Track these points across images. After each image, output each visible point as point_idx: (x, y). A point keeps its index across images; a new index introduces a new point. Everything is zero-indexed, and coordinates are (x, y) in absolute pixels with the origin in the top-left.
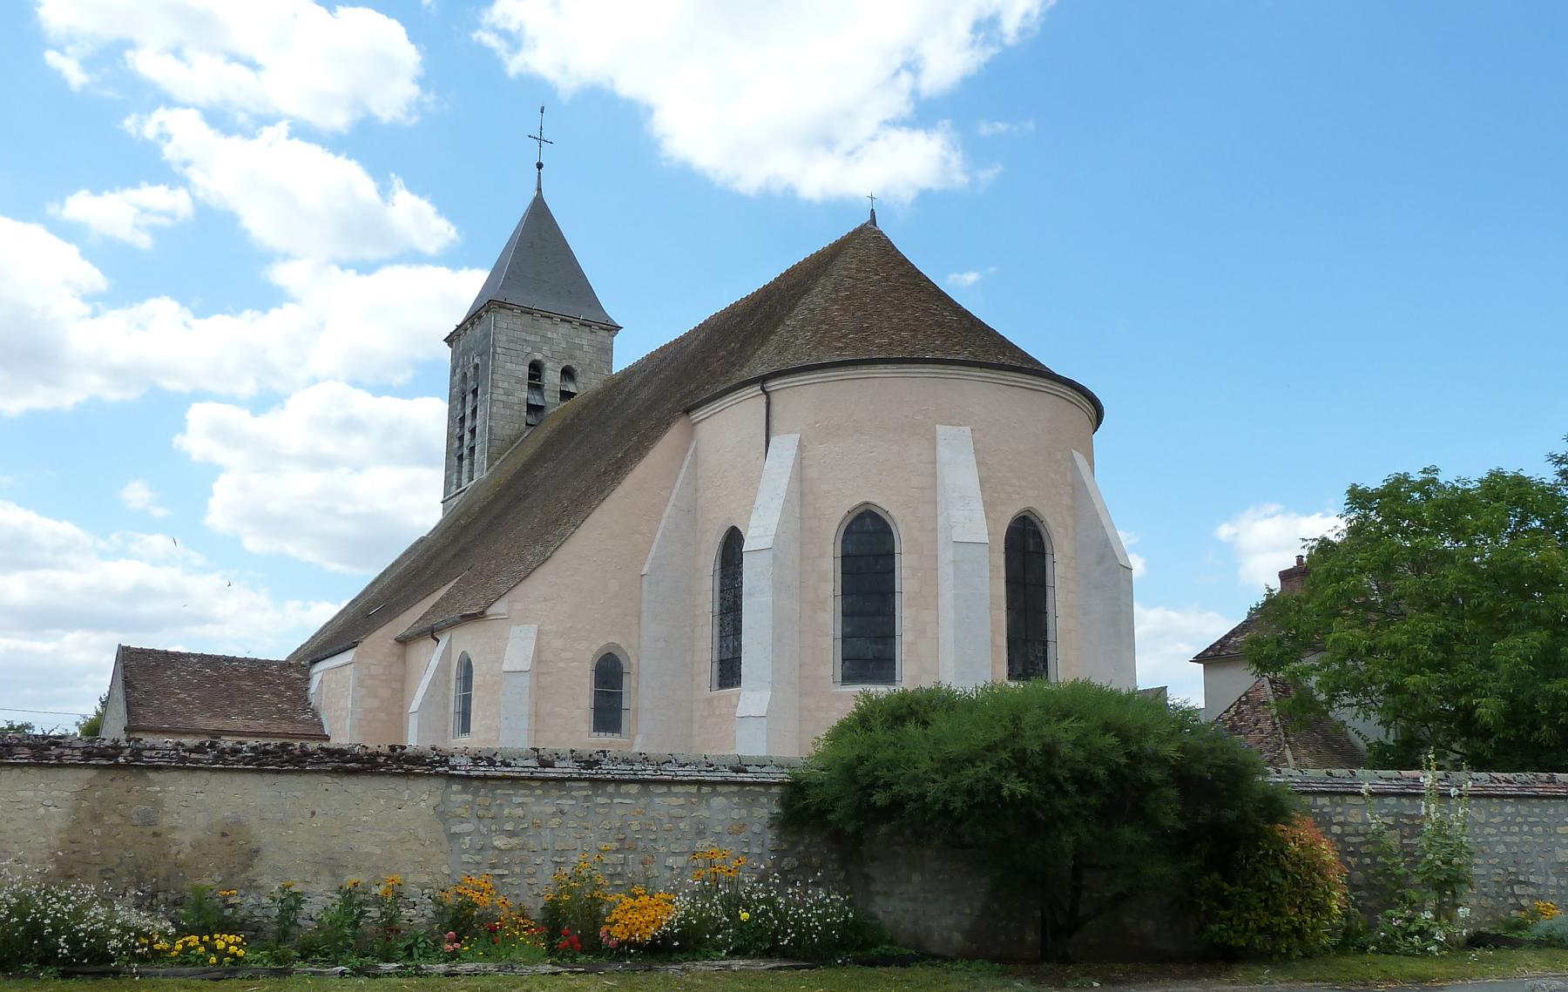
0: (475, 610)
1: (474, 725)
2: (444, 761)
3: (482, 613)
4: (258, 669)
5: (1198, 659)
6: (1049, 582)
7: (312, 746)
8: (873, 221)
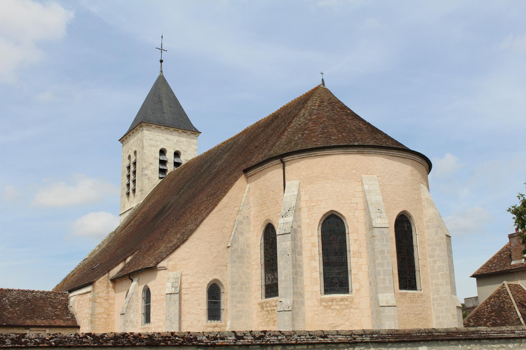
0: (151, 265)
1: (152, 319)
2: (195, 338)
3: (155, 266)
4: (45, 296)
5: (473, 276)
6: (414, 244)
7: (66, 333)
8: (323, 84)
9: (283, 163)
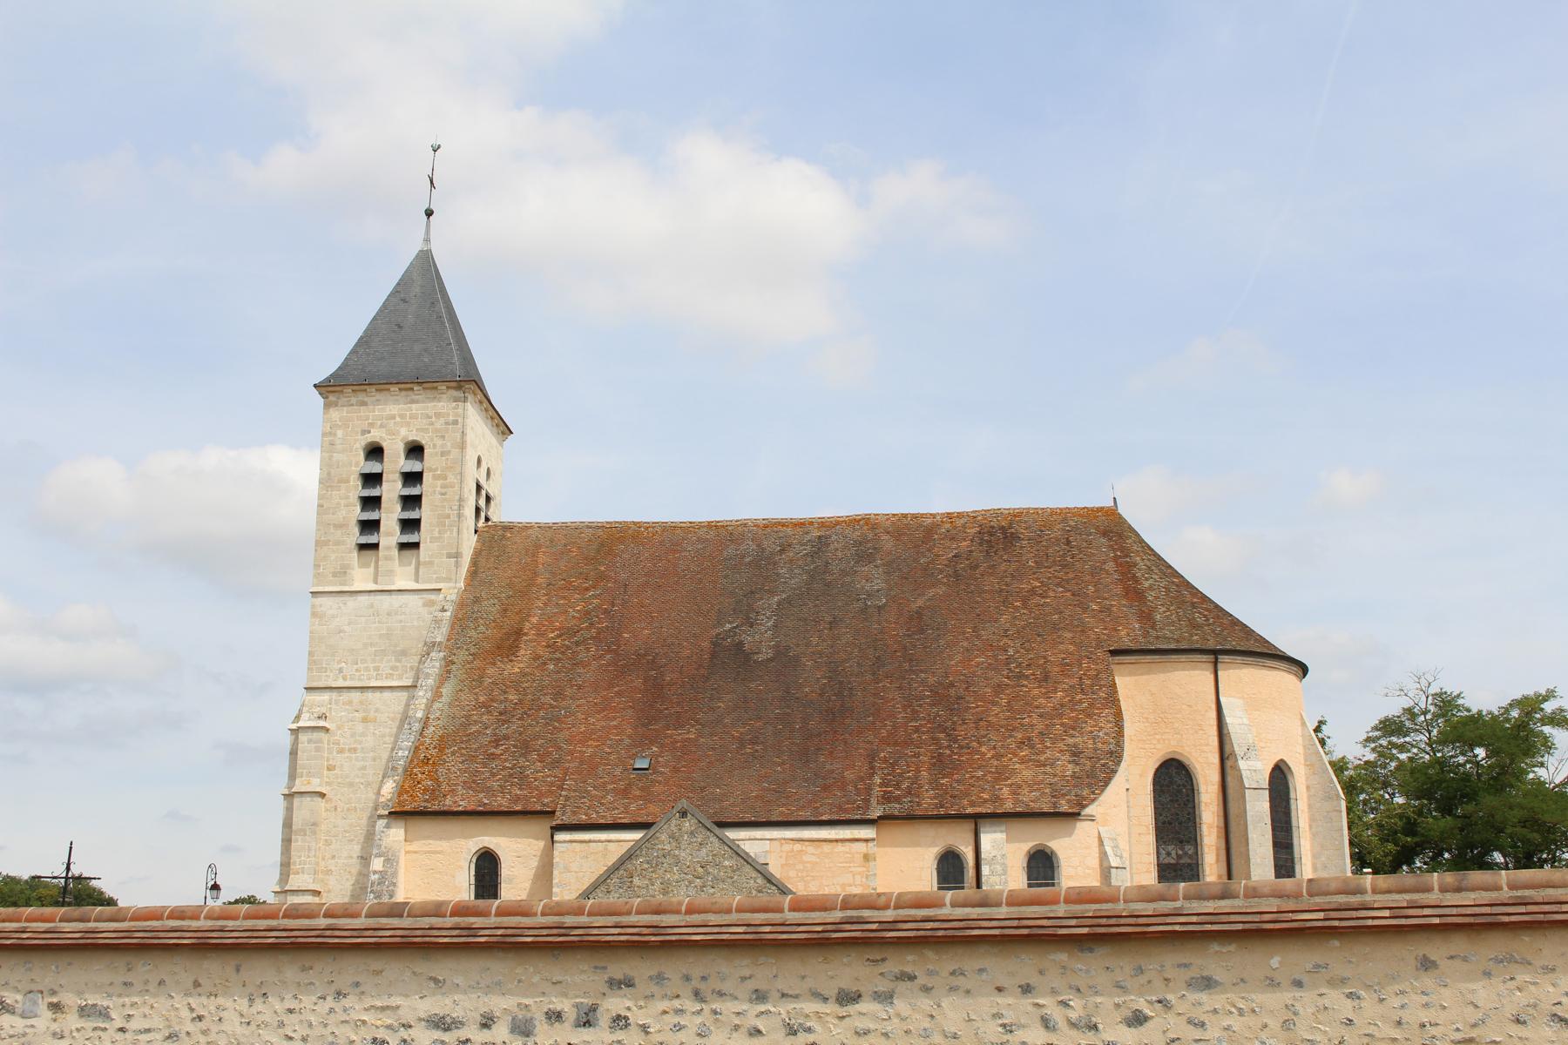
9: (1216, 663)
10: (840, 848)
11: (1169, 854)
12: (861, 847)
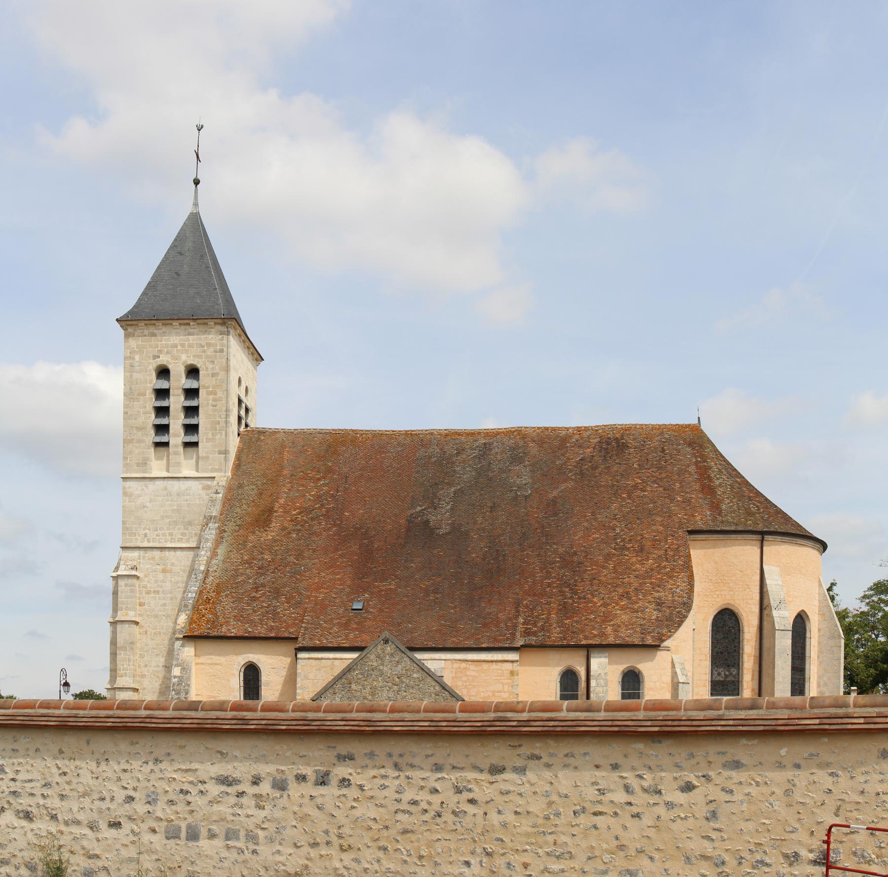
9: (762, 541)
10: (494, 666)
11: (719, 674)
12: (508, 666)
